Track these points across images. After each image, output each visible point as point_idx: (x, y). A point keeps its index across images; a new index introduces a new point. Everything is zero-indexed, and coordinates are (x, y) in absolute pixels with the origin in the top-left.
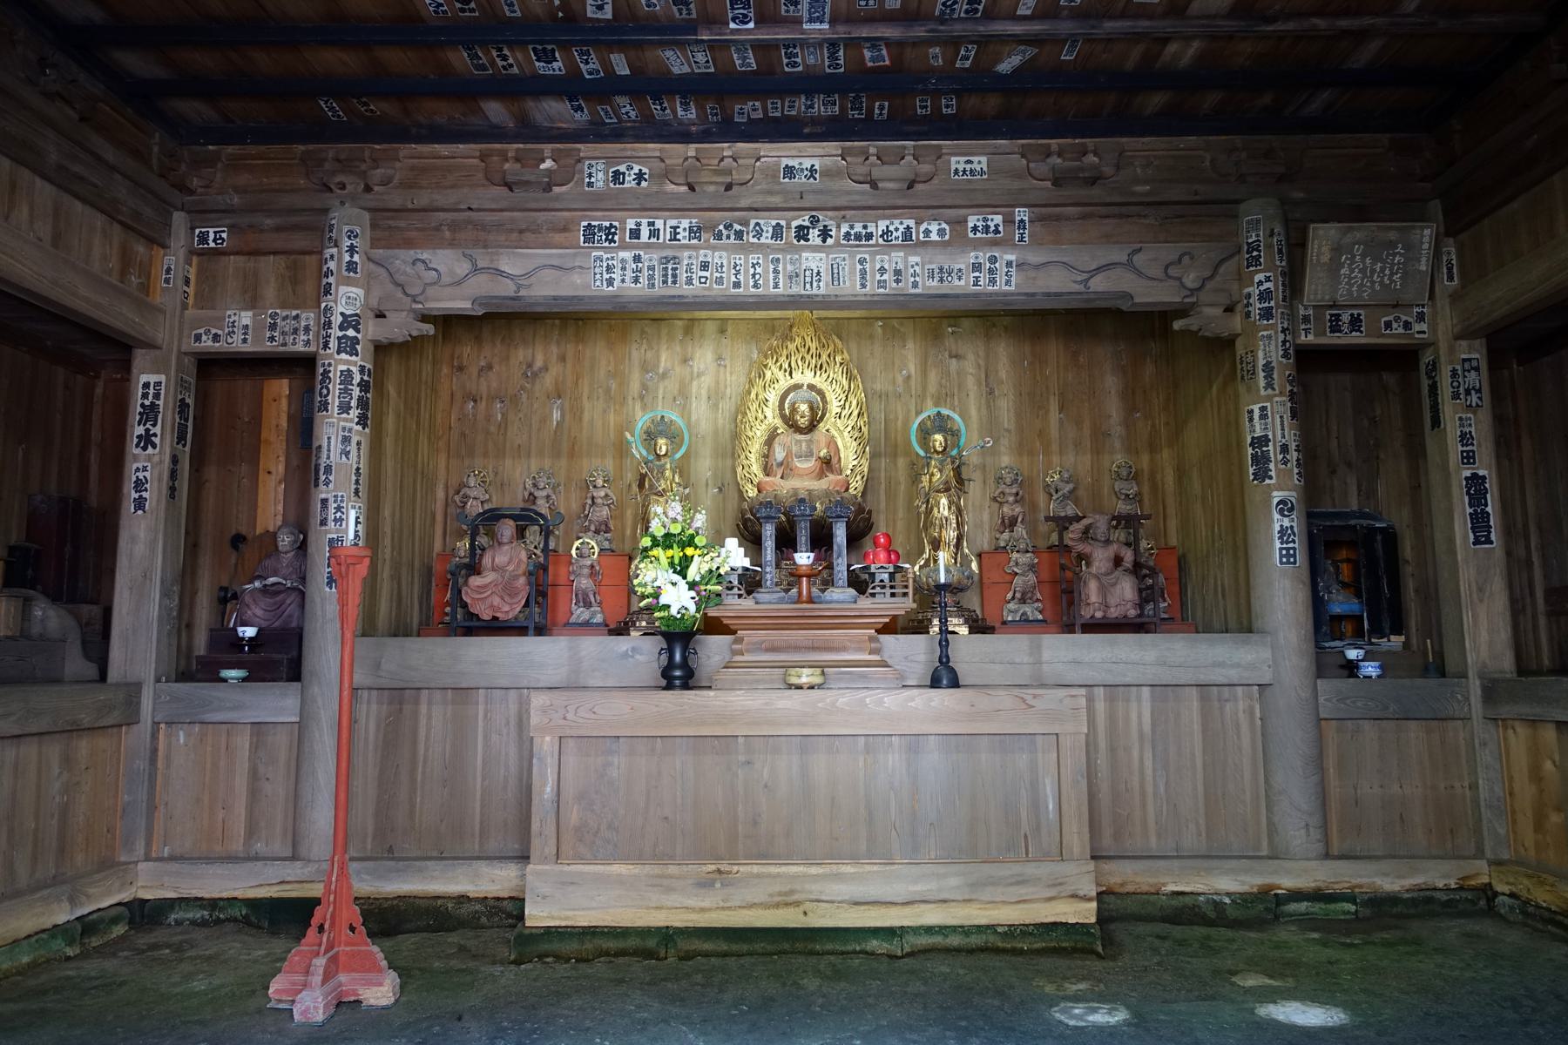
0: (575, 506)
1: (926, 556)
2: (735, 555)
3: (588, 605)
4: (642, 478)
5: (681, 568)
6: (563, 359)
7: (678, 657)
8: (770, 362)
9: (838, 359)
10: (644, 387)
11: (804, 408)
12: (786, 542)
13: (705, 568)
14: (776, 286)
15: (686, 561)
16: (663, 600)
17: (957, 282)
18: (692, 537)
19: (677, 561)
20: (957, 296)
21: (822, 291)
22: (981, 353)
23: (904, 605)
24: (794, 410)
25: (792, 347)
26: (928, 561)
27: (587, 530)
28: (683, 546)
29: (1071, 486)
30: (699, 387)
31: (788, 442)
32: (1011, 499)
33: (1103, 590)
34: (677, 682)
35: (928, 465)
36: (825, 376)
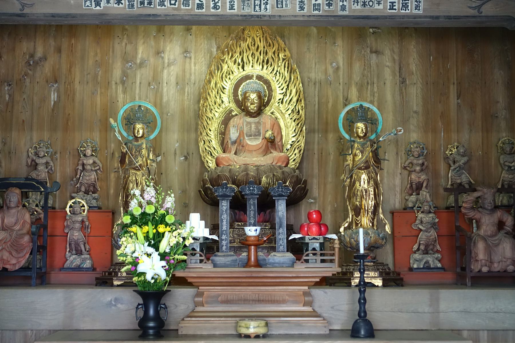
0: (69, 170)
1: (349, 220)
2: (197, 227)
3: (79, 253)
4: (123, 156)
5: (154, 242)
6: (59, 50)
7: (151, 312)
8: (226, 57)
9: (281, 56)
10: (125, 74)
11: (253, 96)
12: (238, 205)
13: (173, 242)
14: (232, 8)
15: (159, 236)
16: (140, 268)
17: (376, 7)
18: (163, 216)
19: (151, 236)
20: (377, 18)
21: (269, 12)
22: (396, 50)
23: (332, 269)
24: (245, 98)
25: (244, 45)
26: (350, 224)
27: (78, 191)
28: (156, 225)
29: (465, 159)
30: (169, 74)
31: (240, 124)
32: (418, 168)
33: (489, 250)
34: (151, 332)
35: (352, 147)
36: (270, 69)
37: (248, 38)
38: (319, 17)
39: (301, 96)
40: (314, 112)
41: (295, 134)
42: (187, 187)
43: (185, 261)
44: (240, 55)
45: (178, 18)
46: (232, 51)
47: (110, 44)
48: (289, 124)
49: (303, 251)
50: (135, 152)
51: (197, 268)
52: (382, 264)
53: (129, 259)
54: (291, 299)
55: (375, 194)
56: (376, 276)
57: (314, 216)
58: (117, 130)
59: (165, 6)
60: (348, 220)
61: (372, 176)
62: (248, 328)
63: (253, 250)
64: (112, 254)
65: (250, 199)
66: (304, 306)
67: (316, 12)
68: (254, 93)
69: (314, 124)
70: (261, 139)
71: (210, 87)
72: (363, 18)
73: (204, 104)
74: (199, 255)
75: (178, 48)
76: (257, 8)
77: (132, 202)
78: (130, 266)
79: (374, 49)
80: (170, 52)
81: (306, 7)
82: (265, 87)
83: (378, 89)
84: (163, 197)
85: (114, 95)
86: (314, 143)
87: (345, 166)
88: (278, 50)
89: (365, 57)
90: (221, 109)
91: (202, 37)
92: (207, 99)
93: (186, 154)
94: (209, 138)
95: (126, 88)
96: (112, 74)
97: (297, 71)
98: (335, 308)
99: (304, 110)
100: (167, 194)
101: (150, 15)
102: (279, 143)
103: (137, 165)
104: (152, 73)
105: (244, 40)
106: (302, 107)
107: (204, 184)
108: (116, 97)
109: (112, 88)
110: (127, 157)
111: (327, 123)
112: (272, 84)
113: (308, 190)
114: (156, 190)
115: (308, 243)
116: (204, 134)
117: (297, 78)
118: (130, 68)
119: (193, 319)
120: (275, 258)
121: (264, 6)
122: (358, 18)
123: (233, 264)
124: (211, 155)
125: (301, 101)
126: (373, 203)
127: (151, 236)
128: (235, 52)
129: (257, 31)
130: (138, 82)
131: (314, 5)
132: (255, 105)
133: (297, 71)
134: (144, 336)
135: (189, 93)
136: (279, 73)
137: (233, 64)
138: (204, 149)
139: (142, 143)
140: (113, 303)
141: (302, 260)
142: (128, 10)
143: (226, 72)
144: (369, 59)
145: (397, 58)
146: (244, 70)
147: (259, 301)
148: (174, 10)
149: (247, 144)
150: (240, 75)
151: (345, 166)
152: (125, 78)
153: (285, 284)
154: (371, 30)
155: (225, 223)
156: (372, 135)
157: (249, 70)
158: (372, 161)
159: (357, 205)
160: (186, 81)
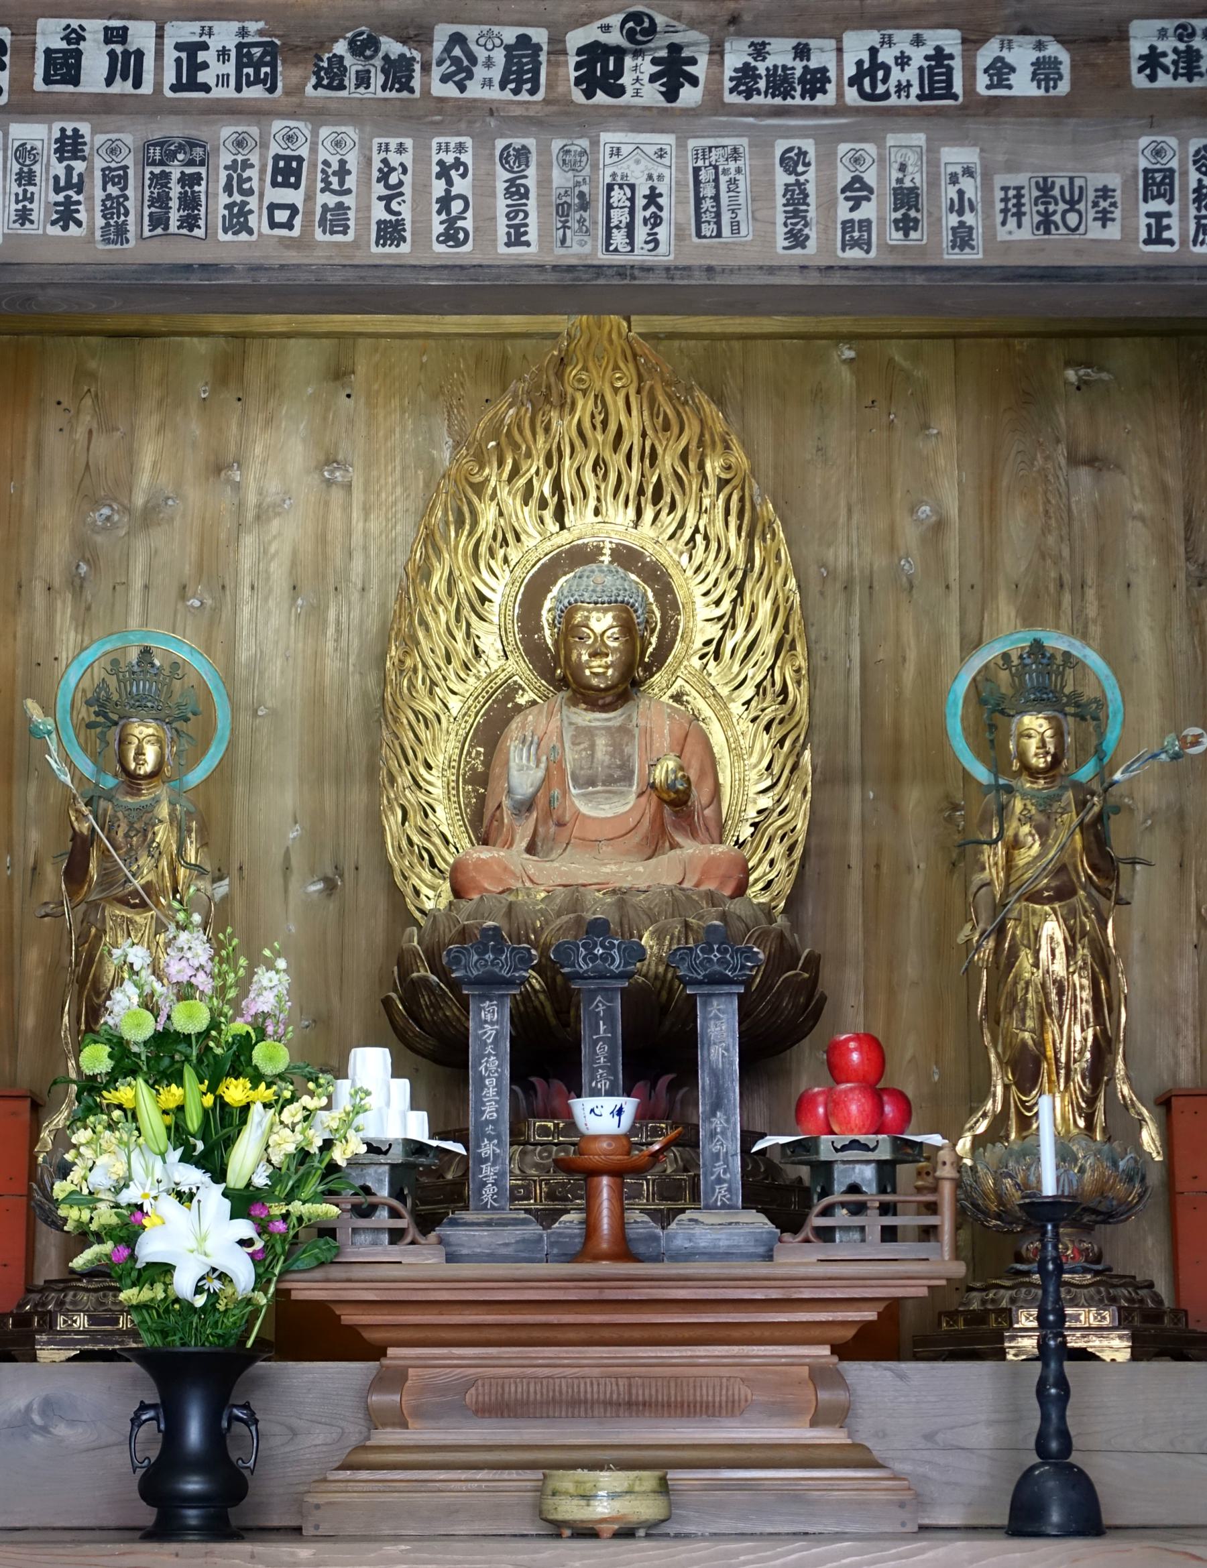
1: (994, 1105)
2: (379, 1101)
4: (81, 846)
7: (194, 1433)
9: (713, 467)
10: (85, 551)
11: (602, 623)
13: (286, 1144)
14: (517, 237)
15: (226, 1123)
16: (150, 1249)
17: (1095, 231)
18: (244, 1045)
19: (193, 1122)
20: (1097, 275)
21: (666, 254)
23: (929, 1267)
24: (569, 630)
25: (563, 426)
26: (999, 1121)
28: (215, 1073)
30: (263, 551)
31: (549, 737)
34: (192, 1515)
35: (1003, 811)
36: (669, 522)
37: (579, 395)
38: (866, 274)
39: (795, 628)
40: (847, 703)
41: (768, 783)
42: (335, 1000)
43: (327, 1232)
44: (549, 463)
45: (304, 278)
46: (516, 447)
47: (25, 433)
48: (745, 743)
49: (811, 1199)
50: (126, 835)
51: (385, 1265)
52: (1130, 1281)
53: (105, 1216)
54: (759, 1397)
55: (1096, 1000)
56: (1106, 1323)
57: (855, 1056)
58: (53, 748)
59: (250, 232)
60: (989, 1106)
61: (1083, 925)
62: (587, 1498)
63: (605, 1194)
64: (42, 1211)
65: (593, 994)
66: (814, 1424)
67: (855, 254)
68: (605, 611)
69: (847, 747)
70: (633, 797)
71: (427, 593)
72: (1041, 278)
73: (402, 662)
74: (385, 1213)
75: (300, 448)
76: (619, 238)
77: (117, 995)
78: (108, 1247)
79: (1083, 450)
80: (264, 462)
81: (812, 232)
82: (650, 594)
83: (1102, 607)
84: (241, 972)
85: (40, 633)
86: (845, 826)
87: (973, 889)
88: (701, 443)
89: (1046, 480)
90: (472, 680)
91: (395, 403)
92: (418, 643)
93: (330, 872)
94: (422, 798)
95: (88, 609)
96: (33, 553)
97: (778, 525)
98: (940, 1438)
99: (805, 683)
100: (255, 961)
101: (188, 268)
102: (707, 812)
103: (137, 883)
104: (192, 549)
105: (562, 406)
106: (798, 671)
107: (404, 974)
108: (51, 643)
109: (31, 608)
110: (94, 853)
111: (897, 745)
112: (677, 581)
113: (823, 999)
114: (217, 946)
115: (829, 1165)
116: (404, 780)
117: (778, 556)
118: (105, 529)
119: (364, 1475)
120: (698, 1230)
121: (647, 229)
122: (1022, 277)
123: (528, 1252)
124: (433, 864)
125: (793, 647)
126: (1090, 1034)
127: (193, 1122)
128: (529, 455)
129: (616, 368)
130: (138, 583)
131: (847, 225)
132: (610, 659)
133: (778, 525)
134: (165, 1529)
135: (344, 626)
136: (706, 537)
137: (518, 500)
138: (404, 843)
139: (157, 801)
140: (37, 1418)
141: (807, 1232)
142: (101, 246)
143: (490, 532)
144: (1063, 489)
145: (1173, 481)
146: (562, 527)
147: (629, 1404)
148: (287, 247)
149: (577, 814)
150: (547, 546)
151: (973, 889)
152: (84, 568)
153: (736, 1334)
154: (1071, 375)
155: (490, 1092)
156: (1078, 766)
157: (582, 524)
158: (1084, 867)
159: (1024, 1043)
160: (331, 580)
